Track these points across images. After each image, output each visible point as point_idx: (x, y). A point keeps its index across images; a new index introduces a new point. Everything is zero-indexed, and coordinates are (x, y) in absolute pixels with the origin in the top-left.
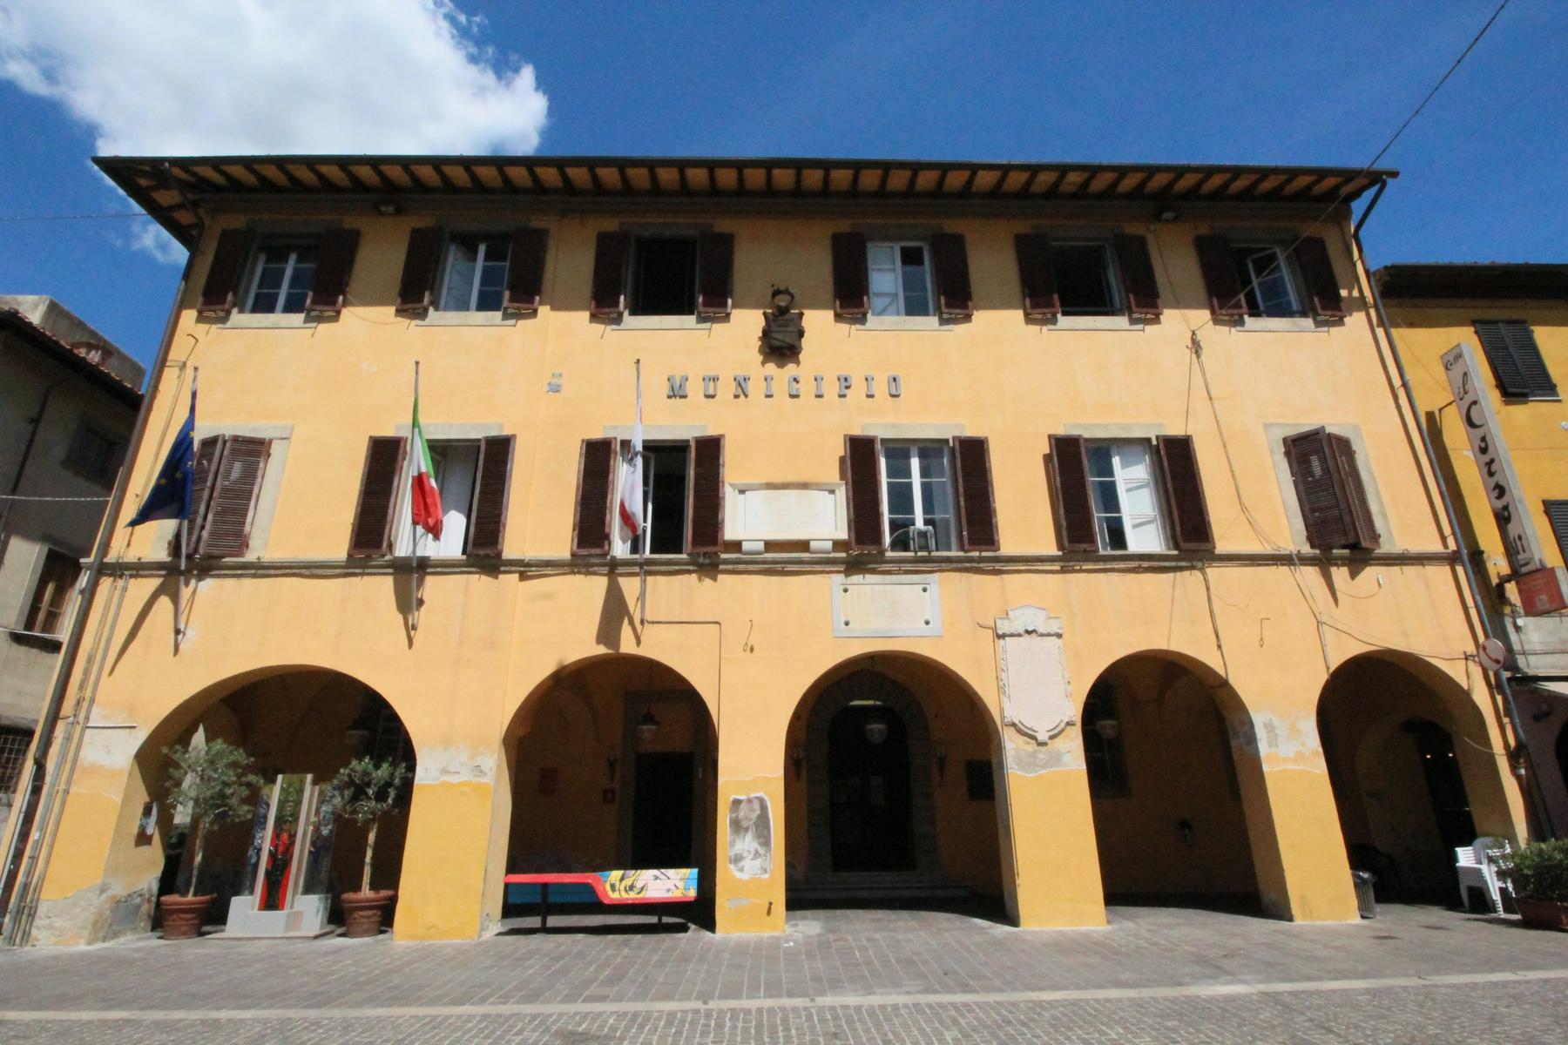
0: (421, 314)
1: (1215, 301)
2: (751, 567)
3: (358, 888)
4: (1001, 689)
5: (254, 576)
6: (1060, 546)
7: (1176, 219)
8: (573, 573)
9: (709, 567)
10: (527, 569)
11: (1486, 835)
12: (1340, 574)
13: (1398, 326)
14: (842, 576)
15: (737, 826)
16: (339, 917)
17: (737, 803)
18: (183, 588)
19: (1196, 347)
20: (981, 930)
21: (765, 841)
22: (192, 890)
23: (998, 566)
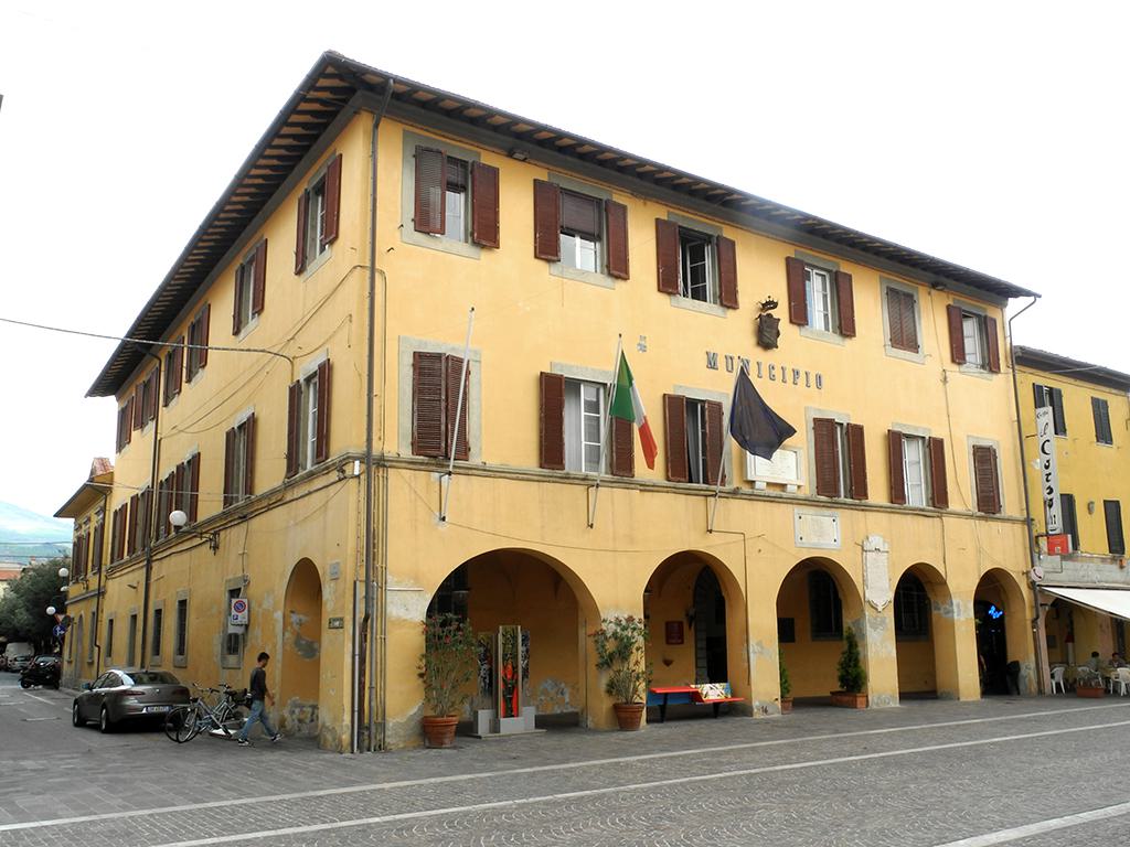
10: (486, 472)
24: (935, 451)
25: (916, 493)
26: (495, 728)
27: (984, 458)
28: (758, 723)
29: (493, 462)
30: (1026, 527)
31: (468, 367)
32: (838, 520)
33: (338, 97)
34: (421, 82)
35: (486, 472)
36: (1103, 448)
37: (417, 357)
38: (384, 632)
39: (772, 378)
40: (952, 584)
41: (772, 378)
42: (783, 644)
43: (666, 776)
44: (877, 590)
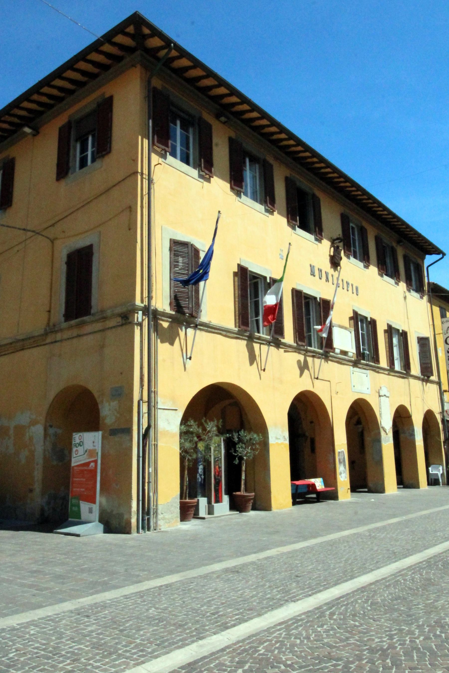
0: (272, 213)
1: (290, 216)
2: (216, 331)
3: (239, 490)
4: (380, 414)
5: (207, 331)
6: (295, 341)
7: (224, 123)
8: (295, 352)
9: (326, 357)
10: (209, 328)
11: (434, 464)
12: (424, 383)
13: (434, 305)
14: (351, 367)
15: (340, 462)
16: (237, 505)
17: (339, 452)
18: (180, 331)
19: (405, 298)
20: (332, 503)
21: (345, 465)
22: (187, 498)
23: (377, 370)
24: (404, 335)
25: (416, 369)
26: (210, 511)
27: (423, 342)
28: (343, 504)
29: (215, 322)
30: (438, 387)
31: (282, 292)
32: (368, 376)
33: (135, 44)
34: (232, 84)
35: (209, 328)
36: (220, 210)
37: (172, 242)
38: (156, 439)
39: (320, 271)
40: (414, 418)
41: (320, 271)
42: (436, 478)
43: (276, 537)
44: (386, 421)
